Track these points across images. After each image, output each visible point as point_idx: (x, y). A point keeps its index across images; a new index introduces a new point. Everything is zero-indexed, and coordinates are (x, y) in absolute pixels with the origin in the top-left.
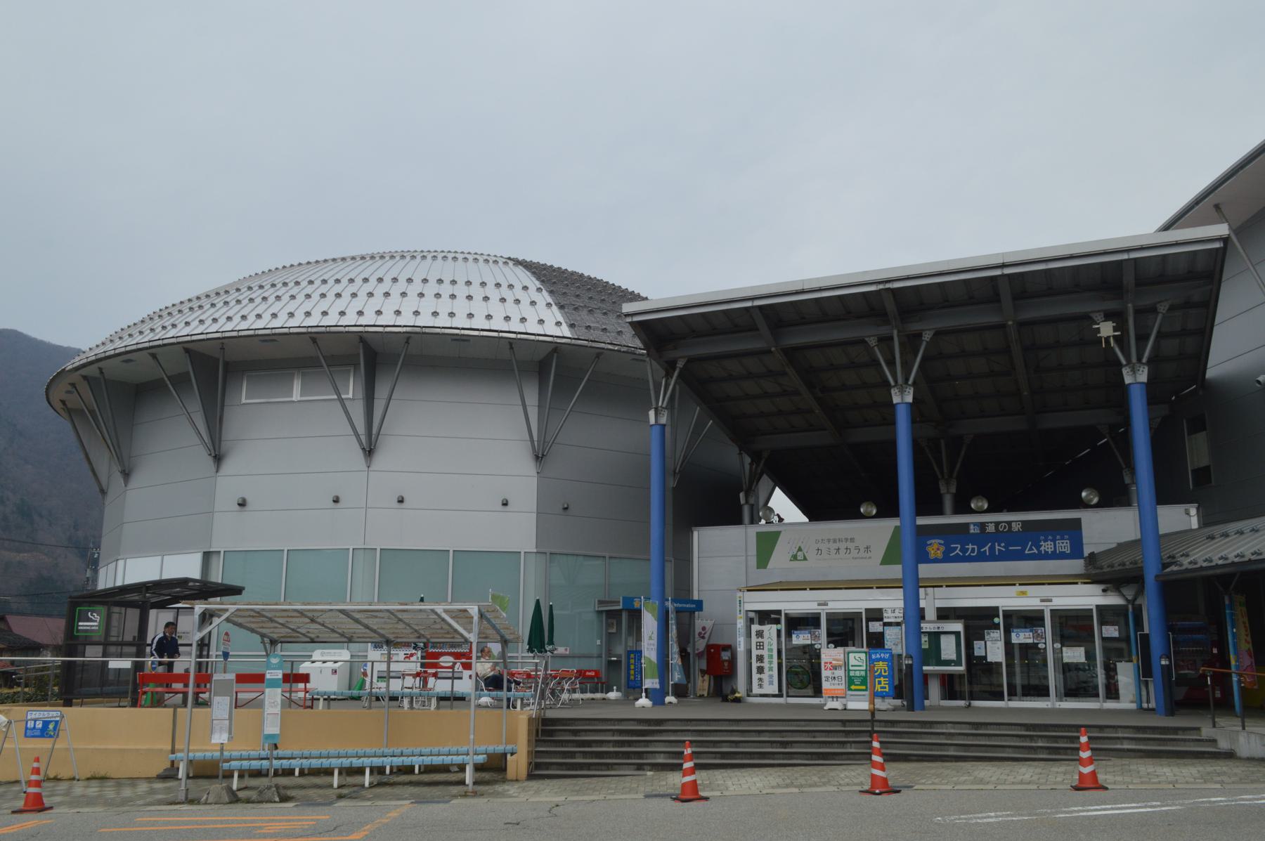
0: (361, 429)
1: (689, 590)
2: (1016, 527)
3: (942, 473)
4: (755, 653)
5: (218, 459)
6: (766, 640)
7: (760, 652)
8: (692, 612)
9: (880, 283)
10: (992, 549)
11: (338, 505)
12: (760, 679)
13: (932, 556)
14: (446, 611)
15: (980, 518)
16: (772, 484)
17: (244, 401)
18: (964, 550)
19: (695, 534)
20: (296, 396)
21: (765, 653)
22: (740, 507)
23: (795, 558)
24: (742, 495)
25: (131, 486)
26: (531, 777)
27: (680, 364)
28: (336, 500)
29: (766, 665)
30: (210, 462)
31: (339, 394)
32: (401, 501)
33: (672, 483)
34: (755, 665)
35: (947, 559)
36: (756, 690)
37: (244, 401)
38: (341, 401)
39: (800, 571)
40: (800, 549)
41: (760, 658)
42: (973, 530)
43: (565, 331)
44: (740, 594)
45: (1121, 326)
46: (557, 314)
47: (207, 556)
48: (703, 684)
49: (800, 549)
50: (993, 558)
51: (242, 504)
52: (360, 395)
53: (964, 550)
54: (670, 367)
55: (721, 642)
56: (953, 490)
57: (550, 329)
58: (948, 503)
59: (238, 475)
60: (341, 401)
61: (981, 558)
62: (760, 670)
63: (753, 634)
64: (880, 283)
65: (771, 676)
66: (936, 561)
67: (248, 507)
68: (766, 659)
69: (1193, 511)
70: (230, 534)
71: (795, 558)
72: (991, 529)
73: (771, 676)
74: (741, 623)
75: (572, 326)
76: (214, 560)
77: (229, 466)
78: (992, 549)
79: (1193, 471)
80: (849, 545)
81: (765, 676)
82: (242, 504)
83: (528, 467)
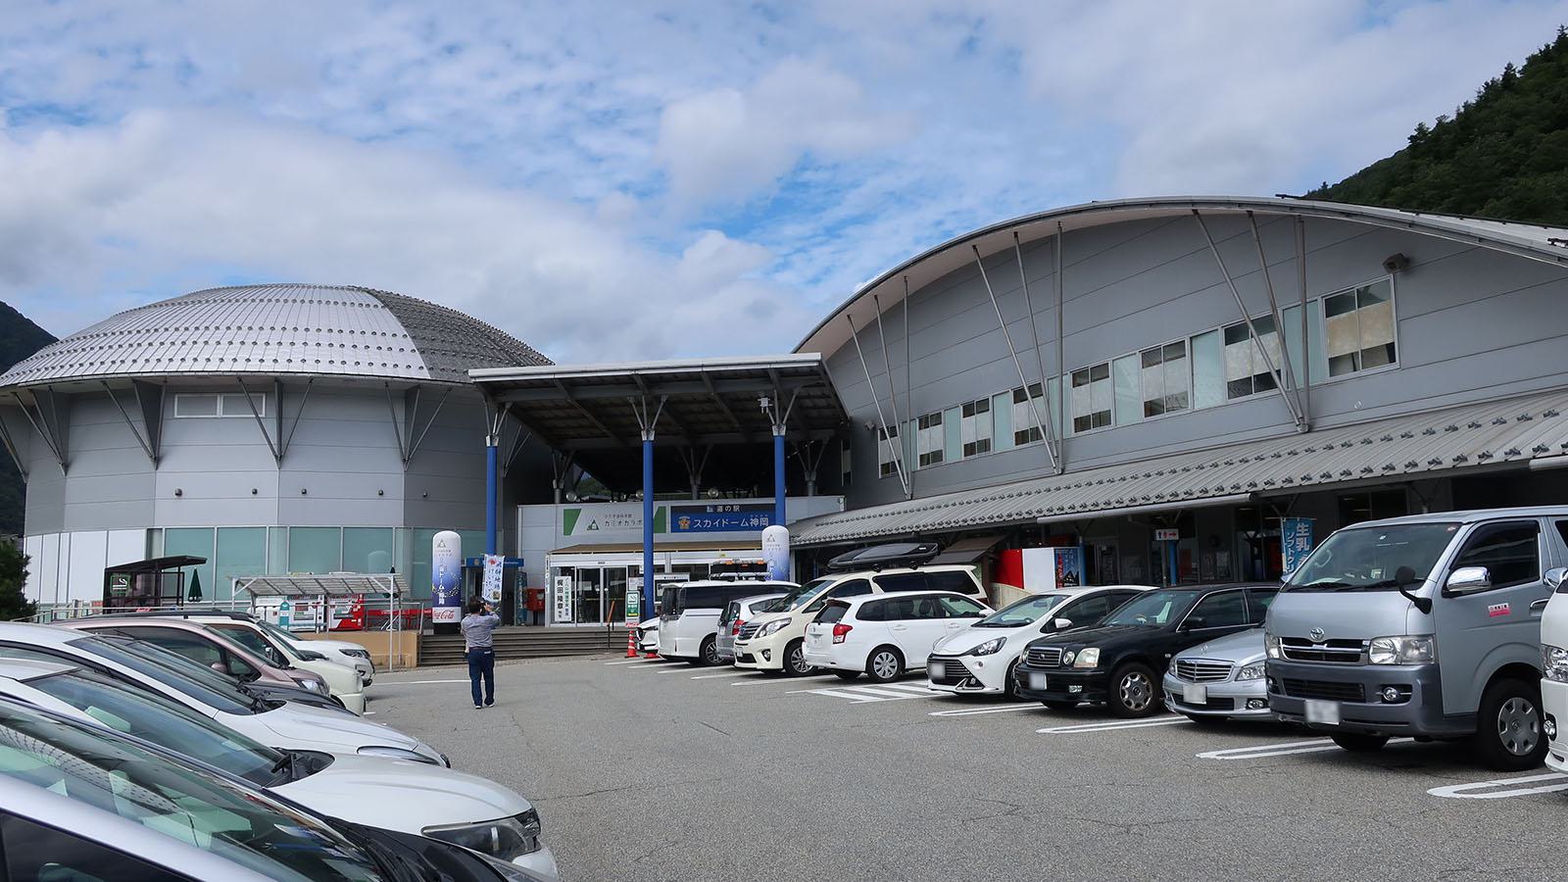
0: (274, 440)
1: (515, 551)
2: (736, 509)
3: (775, 420)
4: (557, 595)
5: (157, 460)
6: (564, 586)
7: (560, 594)
8: (516, 567)
9: (632, 370)
10: (720, 523)
11: (257, 496)
12: (560, 612)
13: (682, 528)
14: (379, 580)
15: (712, 501)
16: (580, 470)
17: (176, 416)
18: (703, 523)
19: (520, 510)
20: (220, 413)
21: (564, 595)
22: (553, 491)
23: (590, 528)
24: (554, 482)
25: (70, 474)
26: (418, 666)
27: (508, 406)
28: (255, 492)
29: (564, 602)
30: (149, 462)
31: (257, 416)
32: (304, 493)
33: (502, 474)
34: (557, 603)
35: (691, 529)
36: (557, 619)
37: (176, 416)
38: (259, 419)
39: (594, 537)
40: (594, 522)
41: (560, 599)
42: (709, 510)
43: (426, 375)
44: (547, 556)
45: (771, 400)
46: (417, 360)
47: (150, 532)
48: (530, 618)
49: (594, 522)
50: (721, 529)
51: (179, 494)
52: (274, 415)
53: (703, 523)
54: (502, 406)
55: (536, 588)
56: (699, 482)
57: (415, 373)
58: (695, 495)
59: (171, 473)
60: (259, 419)
61: (713, 529)
62: (560, 606)
63: (556, 582)
64: (632, 370)
65: (567, 610)
66: (684, 531)
67: (183, 496)
68: (564, 599)
69: (842, 500)
70: (169, 515)
71: (590, 528)
72: (720, 509)
73: (567, 610)
74: (547, 576)
75: (430, 369)
76: (156, 535)
77: (164, 466)
78: (720, 523)
79: (845, 474)
80: (628, 519)
81: (563, 610)
82: (179, 494)
83: (400, 468)
